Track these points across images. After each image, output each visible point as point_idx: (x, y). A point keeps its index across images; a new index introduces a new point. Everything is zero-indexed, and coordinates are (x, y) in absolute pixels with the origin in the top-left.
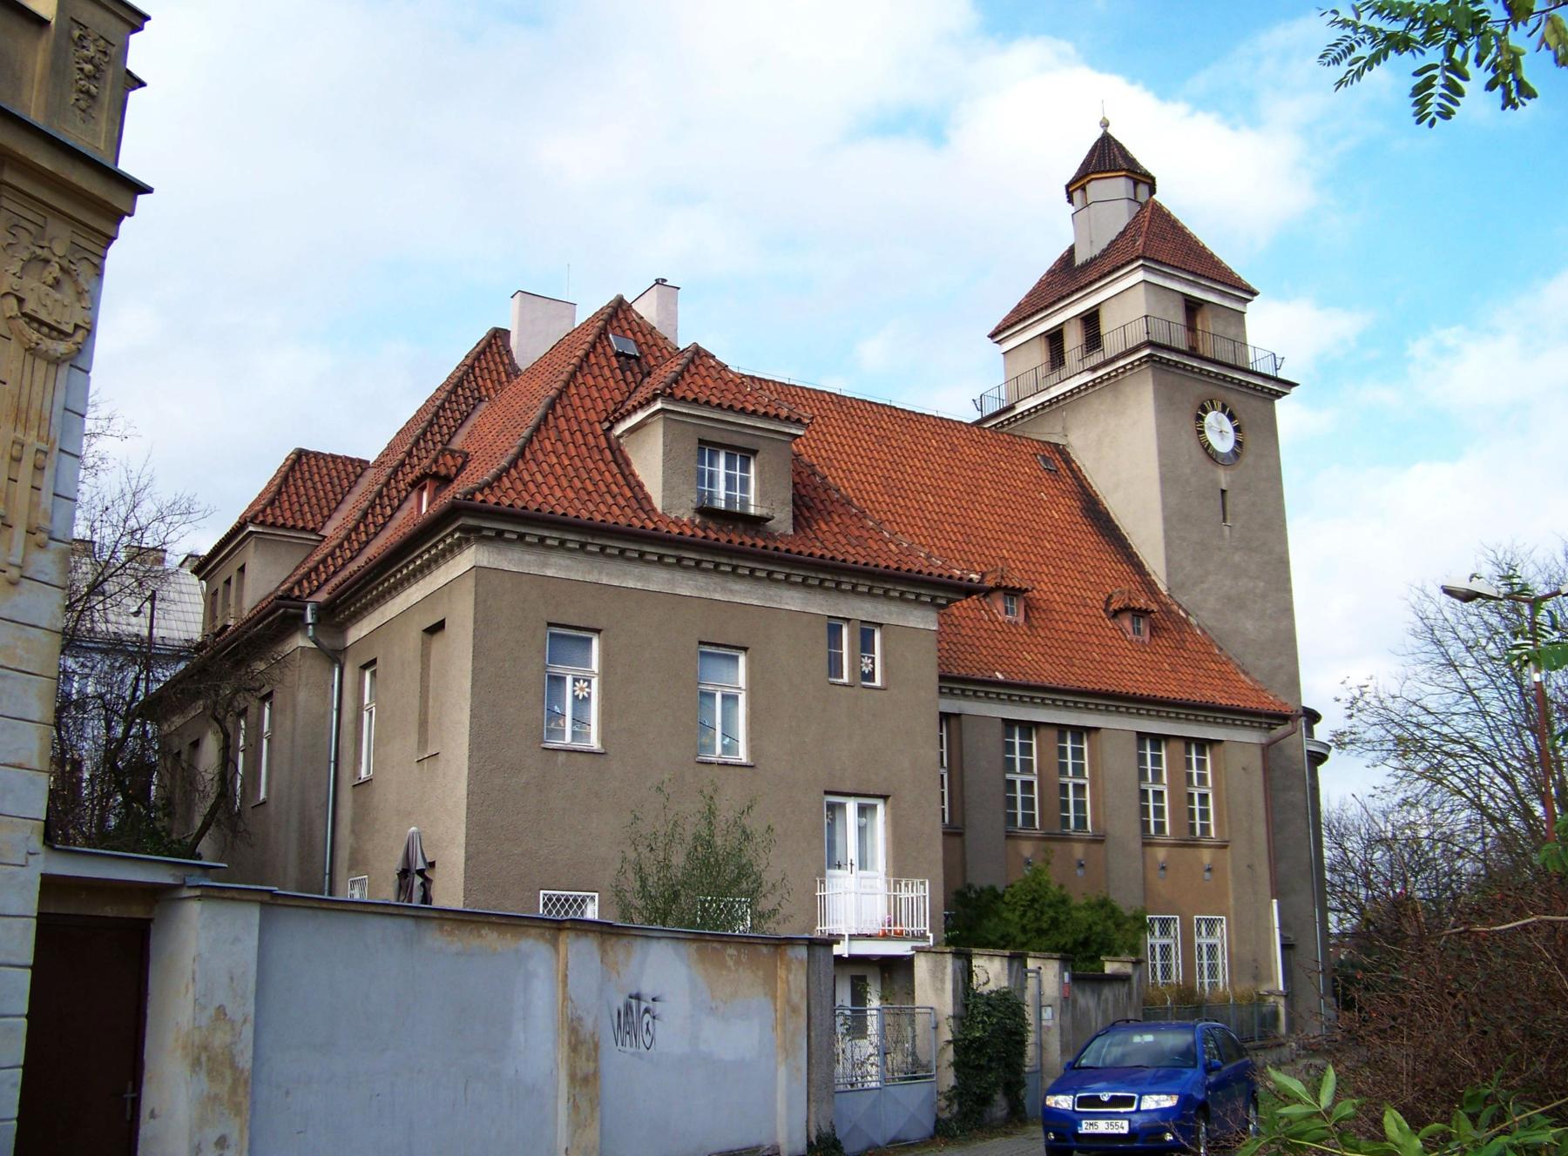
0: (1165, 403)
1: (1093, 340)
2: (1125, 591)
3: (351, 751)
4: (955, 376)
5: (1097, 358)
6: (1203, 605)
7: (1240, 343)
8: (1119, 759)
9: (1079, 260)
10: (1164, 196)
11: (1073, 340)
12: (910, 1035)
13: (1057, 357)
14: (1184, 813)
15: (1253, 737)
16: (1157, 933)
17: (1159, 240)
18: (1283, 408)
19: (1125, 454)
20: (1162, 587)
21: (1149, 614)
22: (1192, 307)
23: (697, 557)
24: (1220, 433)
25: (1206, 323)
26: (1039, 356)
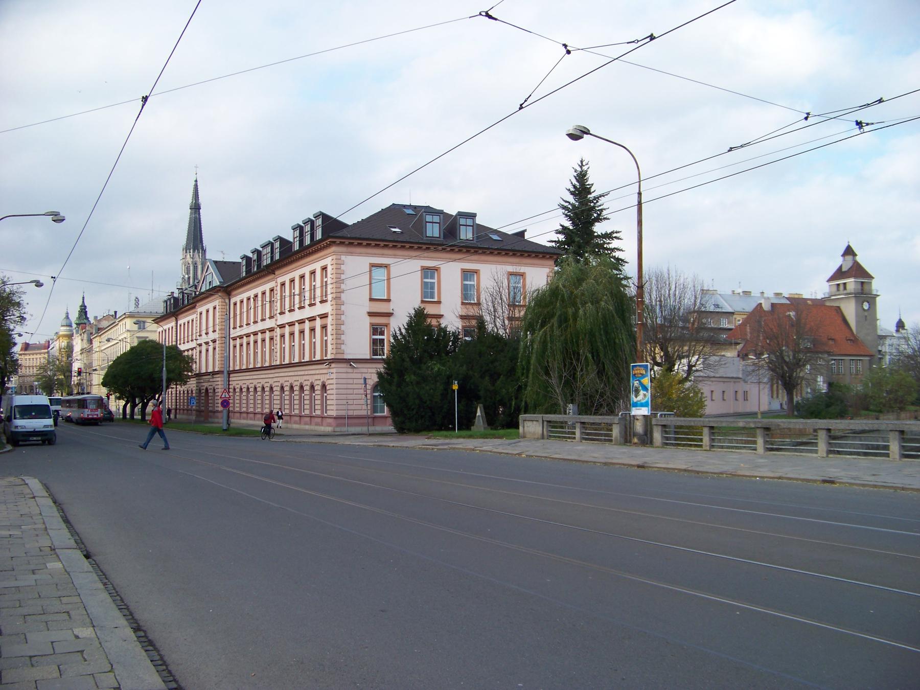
0: (857, 302)
1: (845, 288)
6: (861, 336)
7: (871, 290)
9: (844, 269)
10: (858, 259)
11: (841, 287)
13: (838, 290)
14: (857, 371)
16: (472, 283)
17: (858, 271)
18: (878, 299)
19: (850, 310)
22: (862, 283)
25: (866, 287)
26: (835, 289)
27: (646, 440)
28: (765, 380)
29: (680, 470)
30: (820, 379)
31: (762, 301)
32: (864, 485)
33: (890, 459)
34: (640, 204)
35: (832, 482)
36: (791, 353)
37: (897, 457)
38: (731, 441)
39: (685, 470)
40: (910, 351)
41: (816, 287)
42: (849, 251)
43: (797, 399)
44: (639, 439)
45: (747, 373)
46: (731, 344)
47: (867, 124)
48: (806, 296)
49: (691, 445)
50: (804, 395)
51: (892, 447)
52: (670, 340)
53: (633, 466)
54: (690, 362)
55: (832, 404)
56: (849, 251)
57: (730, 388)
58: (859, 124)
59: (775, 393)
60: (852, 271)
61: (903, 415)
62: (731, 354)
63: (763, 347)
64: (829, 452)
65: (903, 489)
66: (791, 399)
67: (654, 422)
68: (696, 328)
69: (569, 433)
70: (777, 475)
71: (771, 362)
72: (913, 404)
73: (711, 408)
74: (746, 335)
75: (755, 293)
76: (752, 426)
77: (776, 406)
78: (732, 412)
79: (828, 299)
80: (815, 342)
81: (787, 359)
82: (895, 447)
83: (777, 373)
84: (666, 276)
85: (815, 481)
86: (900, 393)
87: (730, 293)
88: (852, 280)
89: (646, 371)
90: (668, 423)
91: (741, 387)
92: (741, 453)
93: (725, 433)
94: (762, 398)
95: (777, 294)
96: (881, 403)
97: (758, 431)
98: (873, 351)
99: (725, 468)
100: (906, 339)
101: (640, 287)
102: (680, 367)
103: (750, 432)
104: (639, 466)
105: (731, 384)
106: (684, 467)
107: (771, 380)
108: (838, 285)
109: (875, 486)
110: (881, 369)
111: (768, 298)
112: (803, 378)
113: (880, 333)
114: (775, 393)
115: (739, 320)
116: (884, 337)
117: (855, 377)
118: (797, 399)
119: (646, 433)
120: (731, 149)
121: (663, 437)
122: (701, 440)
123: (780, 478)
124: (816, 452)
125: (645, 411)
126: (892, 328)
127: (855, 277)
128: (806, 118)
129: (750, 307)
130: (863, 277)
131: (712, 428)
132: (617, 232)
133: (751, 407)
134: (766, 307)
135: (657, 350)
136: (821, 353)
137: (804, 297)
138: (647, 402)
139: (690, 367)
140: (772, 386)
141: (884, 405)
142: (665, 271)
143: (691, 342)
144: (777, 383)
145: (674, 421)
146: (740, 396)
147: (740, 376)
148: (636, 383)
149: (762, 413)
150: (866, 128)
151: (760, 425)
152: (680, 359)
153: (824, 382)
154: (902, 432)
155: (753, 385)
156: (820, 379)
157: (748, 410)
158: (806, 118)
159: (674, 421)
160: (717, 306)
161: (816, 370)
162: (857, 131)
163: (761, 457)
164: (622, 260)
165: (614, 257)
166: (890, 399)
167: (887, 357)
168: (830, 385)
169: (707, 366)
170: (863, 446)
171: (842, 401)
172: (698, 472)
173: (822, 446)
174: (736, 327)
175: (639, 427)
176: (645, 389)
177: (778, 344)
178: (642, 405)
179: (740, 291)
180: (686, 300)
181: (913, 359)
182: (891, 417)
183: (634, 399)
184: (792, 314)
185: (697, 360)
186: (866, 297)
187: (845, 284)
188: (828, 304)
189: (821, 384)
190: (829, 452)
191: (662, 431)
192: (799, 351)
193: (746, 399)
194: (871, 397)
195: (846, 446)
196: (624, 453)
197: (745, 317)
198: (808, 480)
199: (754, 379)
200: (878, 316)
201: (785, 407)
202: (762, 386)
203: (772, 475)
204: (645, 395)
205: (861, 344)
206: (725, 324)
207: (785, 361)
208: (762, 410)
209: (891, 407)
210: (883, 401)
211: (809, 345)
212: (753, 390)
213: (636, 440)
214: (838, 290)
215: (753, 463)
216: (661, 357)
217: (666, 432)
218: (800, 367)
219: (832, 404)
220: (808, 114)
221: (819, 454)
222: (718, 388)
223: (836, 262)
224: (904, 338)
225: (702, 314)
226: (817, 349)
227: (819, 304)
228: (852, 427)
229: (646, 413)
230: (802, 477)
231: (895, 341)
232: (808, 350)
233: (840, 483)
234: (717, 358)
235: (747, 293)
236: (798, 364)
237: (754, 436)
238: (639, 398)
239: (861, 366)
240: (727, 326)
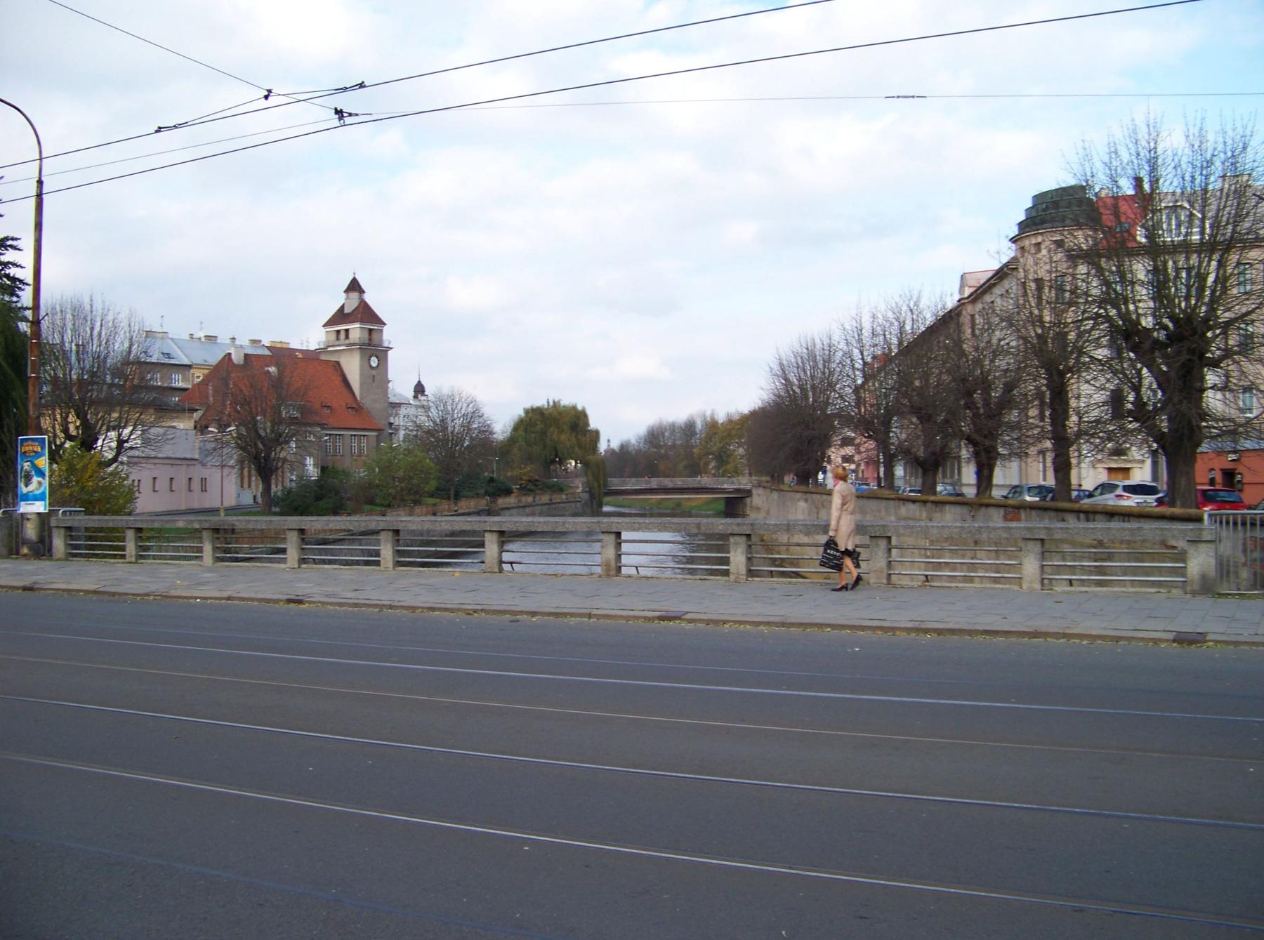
0: (362, 357)
1: (347, 337)
3: (670, 485)
6: (367, 403)
7: (381, 340)
8: (347, 440)
9: (347, 311)
10: (367, 297)
11: (343, 335)
12: (1247, 648)
14: (360, 450)
17: (366, 314)
19: (352, 367)
22: (370, 330)
25: (375, 336)
26: (333, 337)
27: (42, 549)
28: (232, 462)
29: (87, 592)
30: (310, 461)
31: (232, 351)
32: (341, 605)
33: (382, 568)
34: (39, 196)
35: (300, 602)
36: (269, 424)
37: (390, 565)
38: (176, 549)
39: (95, 592)
40: (428, 424)
41: (310, 336)
42: (354, 286)
43: (276, 489)
44: (30, 549)
45: (206, 453)
46: (184, 410)
47: (350, 115)
48: (295, 344)
49: (105, 556)
50: (288, 484)
51: (383, 553)
52: (92, 403)
53: (17, 588)
54: (120, 435)
55: (324, 496)
56: (354, 286)
57: (181, 474)
58: (339, 113)
59: (246, 480)
60: (357, 315)
61: (418, 510)
62: (184, 424)
63: (229, 415)
64: (303, 561)
65: (391, 607)
66: (267, 489)
67: (53, 523)
68: (133, 386)
69: (192, 549)
70: (226, 594)
71: (240, 436)
72: (432, 495)
73: (147, 503)
74: (207, 397)
75: (224, 338)
76: (197, 526)
77: (247, 499)
78: (183, 507)
79: (322, 351)
80: (303, 410)
81: (263, 434)
82: (387, 553)
83: (248, 453)
84: (88, 307)
85: (276, 601)
86: (415, 481)
87: (187, 337)
88: (357, 325)
89: (43, 448)
90: (76, 524)
91: (197, 472)
92: (179, 566)
93: (156, 538)
94: (228, 488)
95: (254, 342)
96: (390, 495)
97: (205, 534)
98: (382, 423)
99: (153, 588)
100: (426, 409)
101: (36, 323)
102: (106, 444)
103: (195, 534)
104: (25, 589)
105: (174, 469)
106: (92, 587)
107: (241, 462)
108: (338, 332)
109: (356, 605)
110: (391, 447)
111: (241, 347)
112: (285, 460)
113: (392, 399)
114: (246, 480)
115: (199, 375)
116: (399, 405)
117: (357, 457)
119: (41, 540)
120: (159, 130)
121: (67, 545)
122: (123, 548)
123: (229, 598)
124: (284, 561)
125: (40, 507)
126: (409, 393)
127: (361, 321)
128: (266, 97)
129: (214, 358)
131: (139, 530)
132: (13, 239)
133: (212, 501)
134: (237, 358)
135: (71, 418)
136: (311, 425)
137: (292, 346)
138: (43, 493)
139: (121, 443)
140: (242, 470)
141: (394, 498)
142: (87, 301)
143: (122, 407)
145: (83, 520)
146: (196, 485)
147: (197, 456)
148: (27, 466)
149: (227, 510)
150: (348, 120)
151: (207, 525)
152: (108, 430)
153: (315, 465)
154: (397, 532)
155: (214, 469)
156: (310, 461)
157: (207, 505)
158: (266, 97)
159: (83, 520)
160: (169, 356)
161: (304, 449)
162: (336, 123)
163: (210, 570)
164: (21, 281)
165: (7, 276)
166: (402, 489)
167: (402, 433)
168: (324, 469)
169: (146, 442)
170: (363, 553)
171: (337, 493)
172: (114, 594)
173: (293, 554)
174: (194, 386)
175: (31, 531)
176: (41, 473)
178: (36, 498)
179: (201, 335)
180: (117, 345)
181: (433, 436)
182: (402, 513)
183: (23, 489)
184: (272, 369)
185: (131, 433)
186: (374, 349)
187: (347, 331)
188: (323, 357)
189: (311, 469)
190: (303, 561)
191: (66, 536)
192: (280, 423)
193: (204, 489)
194: (378, 486)
195: (340, 552)
196: (6, 569)
197: (206, 372)
198: (268, 601)
199: (216, 461)
200: (390, 377)
201: (259, 500)
202: (226, 471)
203: (218, 594)
204: (40, 483)
206: (179, 382)
207: (260, 437)
208: (226, 504)
209: (403, 500)
210: (392, 491)
211: (296, 414)
212: (214, 476)
213: (25, 550)
214: (338, 339)
215: (199, 579)
216: (77, 428)
217: (72, 537)
218: (280, 444)
219: (324, 496)
220: (270, 91)
221: (288, 565)
222: (164, 473)
223: (336, 300)
224: (423, 407)
225: (145, 366)
226: (306, 420)
227: (311, 357)
228: (331, 526)
229: (42, 510)
230: (260, 596)
231: (411, 411)
232: (293, 421)
233: (310, 602)
234: (161, 431)
235: (211, 339)
236: (279, 440)
237: (201, 540)
238: (31, 488)
239: (366, 443)
240: (180, 385)
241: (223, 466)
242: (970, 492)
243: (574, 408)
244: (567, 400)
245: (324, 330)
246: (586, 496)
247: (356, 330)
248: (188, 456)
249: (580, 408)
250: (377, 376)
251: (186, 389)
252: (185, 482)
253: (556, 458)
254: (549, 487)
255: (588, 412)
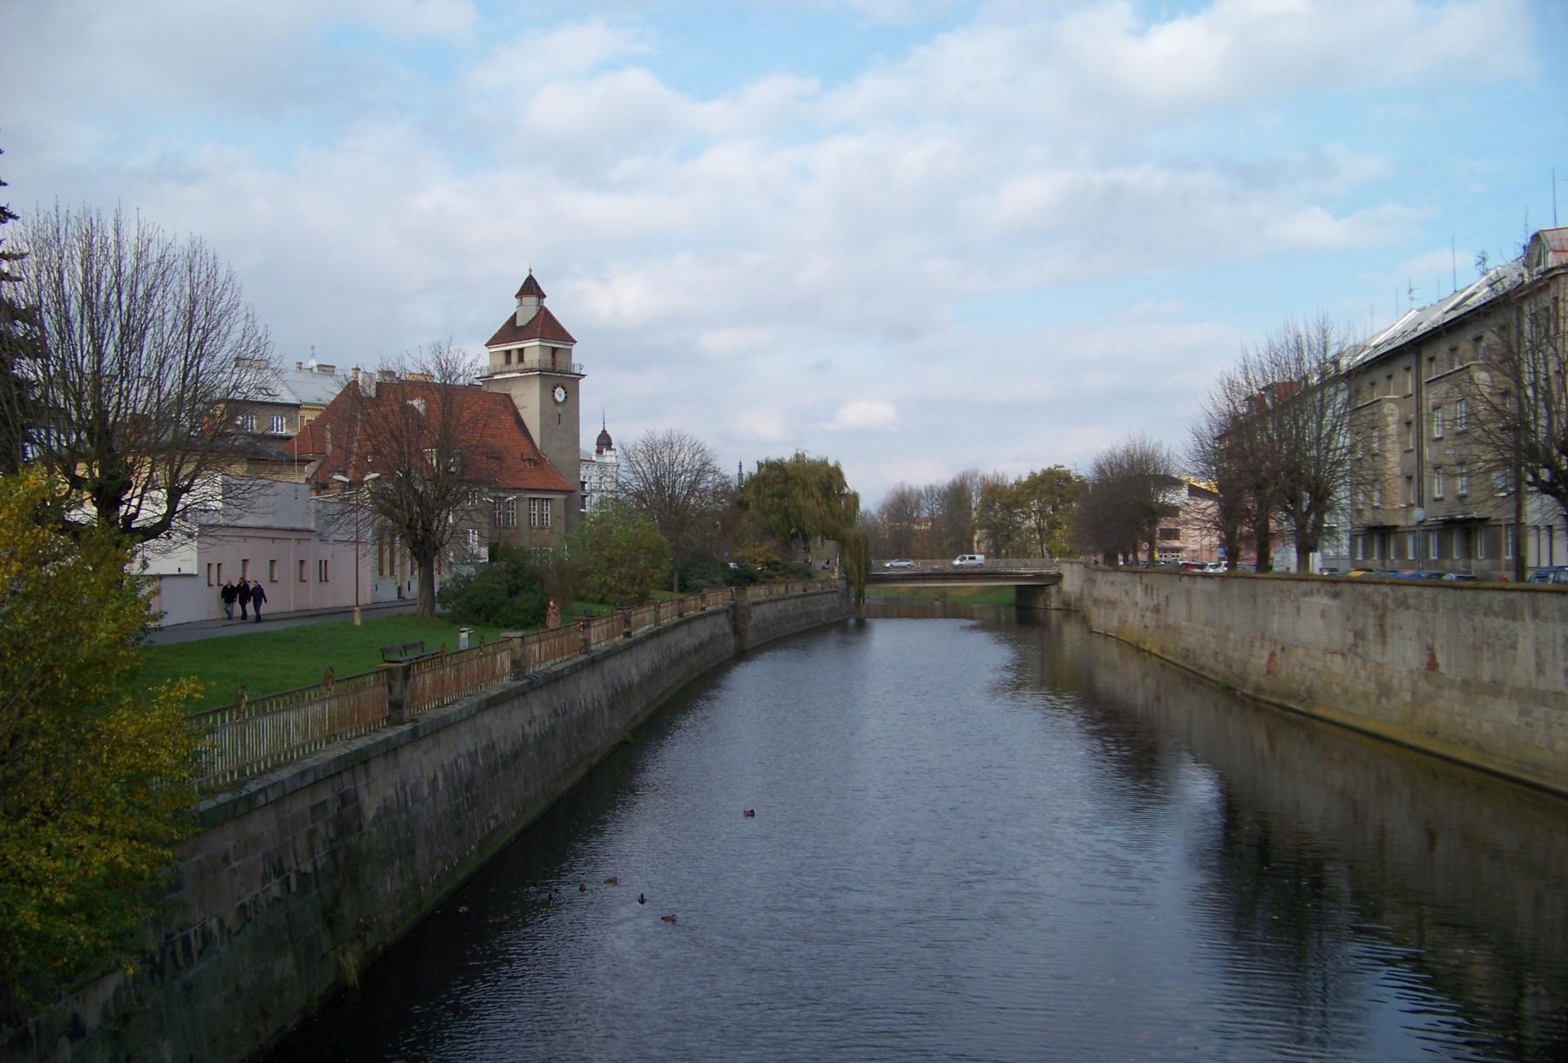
1: (521, 359)
2: (527, 451)
4: (474, 359)
5: (522, 366)
6: (550, 453)
7: (569, 363)
8: (524, 505)
9: (520, 323)
10: (547, 303)
13: (508, 362)
15: (562, 497)
17: (547, 327)
19: (529, 402)
20: (538, 443)
21: (537, 460)
22: (554, 350)
23: (519, 634)
24: (560, 395)
25: (559, 357)
26: (501, 359)
42: (530, 288)
43: (441, 578)
56: (530, 288)
60: (536, 327)
66: (427, 581)
79: (488, 379)
91: (313, 551)
98: (571, 483)
108: (508, 353)
118: (441, 578)
127: (542, 338)
130: (556, 339)
144: (392, 543)
146: (311, 571)
147: (312, 526)
156: (473, 538)
157: (330, 603)
174: (304, 429)
177: (401, 454)
186: (560, 377)
187: (521, 351)
193: (323, 578)
205: (546, 470)
214: (508, 362)
223: (506, 306)
239: (550, 511)
241: (357, 542)
242: (1293, 569)
243: (825, 463)
244: (813, 454)
245: (487, 351)
246: (842, 584)
247: (533, 349)
248: (299, 526)
249: (831, 463)
250: (564, 416)
251: (289, 438)
252: (293, 568)
253: (794, 533)
254: (792, 572)
255: (845, 470)
